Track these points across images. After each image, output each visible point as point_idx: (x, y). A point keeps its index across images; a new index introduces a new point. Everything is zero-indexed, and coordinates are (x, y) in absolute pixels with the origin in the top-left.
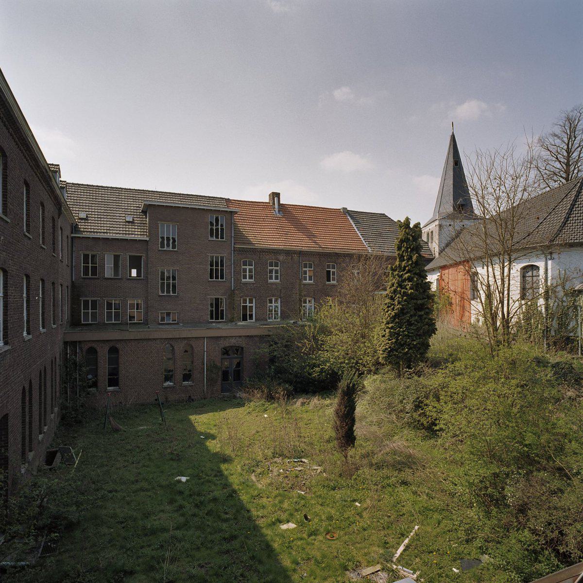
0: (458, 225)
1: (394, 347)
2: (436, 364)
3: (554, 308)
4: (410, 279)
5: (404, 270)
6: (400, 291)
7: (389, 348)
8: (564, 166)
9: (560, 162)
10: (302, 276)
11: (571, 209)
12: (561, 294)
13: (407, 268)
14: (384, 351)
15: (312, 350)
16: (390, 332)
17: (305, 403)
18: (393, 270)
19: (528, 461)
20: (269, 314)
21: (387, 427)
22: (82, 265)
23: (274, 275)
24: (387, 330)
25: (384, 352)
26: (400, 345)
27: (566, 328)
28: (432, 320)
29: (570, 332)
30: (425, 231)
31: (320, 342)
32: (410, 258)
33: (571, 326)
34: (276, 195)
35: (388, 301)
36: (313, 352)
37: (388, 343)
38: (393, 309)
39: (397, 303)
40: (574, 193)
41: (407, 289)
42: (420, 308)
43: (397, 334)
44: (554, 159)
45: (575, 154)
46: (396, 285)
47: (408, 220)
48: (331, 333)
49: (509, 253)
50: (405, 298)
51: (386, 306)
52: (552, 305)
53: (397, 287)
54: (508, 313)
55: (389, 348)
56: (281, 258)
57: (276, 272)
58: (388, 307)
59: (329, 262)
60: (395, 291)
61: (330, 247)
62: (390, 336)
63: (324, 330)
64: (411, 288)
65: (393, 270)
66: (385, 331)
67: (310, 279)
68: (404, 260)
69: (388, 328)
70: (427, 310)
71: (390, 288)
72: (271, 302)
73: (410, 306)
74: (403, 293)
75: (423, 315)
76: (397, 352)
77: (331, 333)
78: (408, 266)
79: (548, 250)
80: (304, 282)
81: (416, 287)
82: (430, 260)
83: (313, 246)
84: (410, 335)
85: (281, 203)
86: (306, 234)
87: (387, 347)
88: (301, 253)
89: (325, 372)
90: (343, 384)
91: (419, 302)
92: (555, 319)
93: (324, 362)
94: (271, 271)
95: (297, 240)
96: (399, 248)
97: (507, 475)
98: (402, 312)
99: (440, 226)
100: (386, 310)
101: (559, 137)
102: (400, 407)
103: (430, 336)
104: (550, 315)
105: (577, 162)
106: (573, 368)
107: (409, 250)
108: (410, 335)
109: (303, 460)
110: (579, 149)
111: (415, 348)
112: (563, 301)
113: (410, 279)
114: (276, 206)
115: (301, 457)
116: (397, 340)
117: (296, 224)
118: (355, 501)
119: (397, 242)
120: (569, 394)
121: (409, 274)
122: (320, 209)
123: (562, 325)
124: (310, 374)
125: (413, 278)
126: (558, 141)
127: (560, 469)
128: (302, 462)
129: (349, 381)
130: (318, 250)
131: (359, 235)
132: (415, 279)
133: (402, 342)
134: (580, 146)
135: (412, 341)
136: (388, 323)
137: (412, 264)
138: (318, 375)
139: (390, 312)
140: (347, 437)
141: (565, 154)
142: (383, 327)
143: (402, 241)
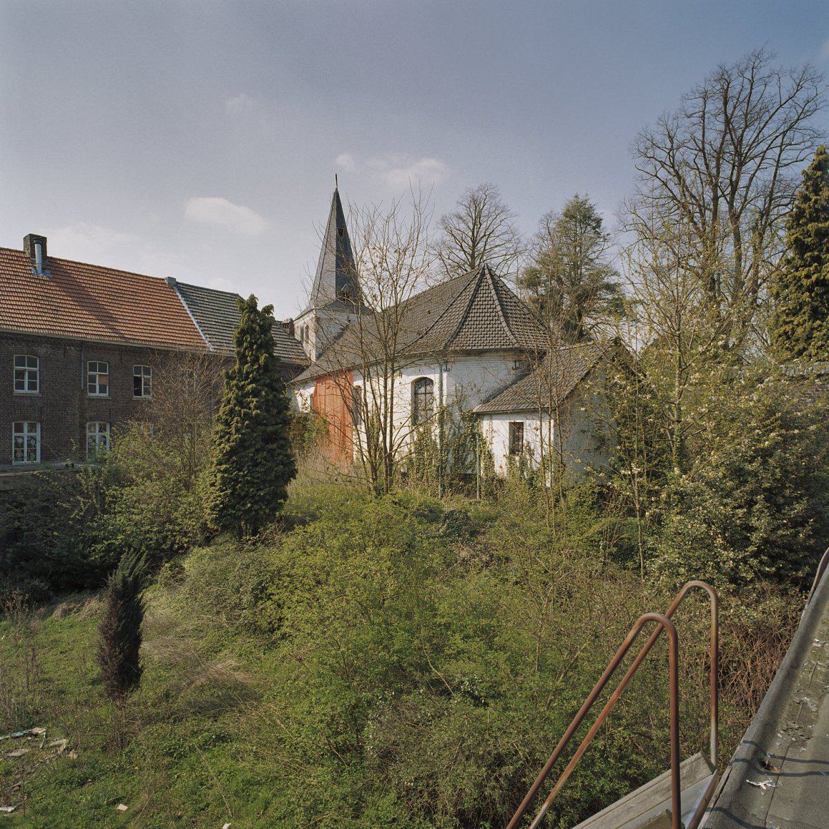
0: (342, 317)
1: (229, 501)
2: (289, 525)
3: (450, 436)
4: (255, 393)
5: (247, 378)
6: (240, 411)
7: (221, 504)
8: (469, 257)
9: (465, 252)
10: (85, 385)
11: (470, 306)
12: (457, 416)
13: (251, 375)
14: (212, 509)
15: (92, 512)
16: (222, 478)
17: (70, 610)
18: (230, 378)
19: (399, 676)
20: (16, 452)
21: (212, 636)
22: (38, 381)
23: (26, 381)
24: (219, 475)
25: (214, 510)
26: (238, 498)
27: (463, 464)
28: (289, 456)
29: (468, 469)
30: (299, 324)
31: (108, 499)
32: (256, 360)
33: (469, 460)
34: (37, 241)
35: (220, 427)
36: (93, 517)
37: (220, 496)
38: (228, 440)
39: (234, 431)
40: (474, 286)
41: (250, 409)
42: (269, 438)
43: (234, 480)
44: (458, 247)
45: (481, 245)
46: (233, 402)
47: (253, 299)
48: (132, 483)
49: (392, 363)
50: (247, 422)
51: (218, 436)
52: (447, 433)
53: (235, 405)
54: (391, 446)
55: (221, 504)
56: (42, 351)
57: (32, 375)
58: (221, 437)
59: (133, 363)
60: (231, 412)
61: (141, 338)
62: (223, 484)
63: (119, 478)
64: (256, 408)
65: (230, 378)
66: (216, 477)
67: (102, 390)
68: (247, 363)
69: (219, 471)
70: (282, 442)
71: (225, 406)
72: (19, 429)
73: (255, 435)
74: (244, 414)
75: (274, 450)
76: (234, 509)
77: (132, 483)
78: (252, 372)
79: (443, 357)
80: (91, 395)
81: (266, 405)
82: (300, 369)
83: (108, 334)
84: (256, 481)
85: (49, 255)
86: (96, 314)
87: (218, 502)
88: (83, 345)
89: (115, 550)
90: (116, 579)
91: (270, 429)
92: (451, 452)
93: (114, 534)
94: (20, 374)
95: (78, 323)
96: (240, 344)
97: (369, 703)
98: (242, 445)
99: (318, 320)
100: (217, 443)
101: (464, 221)
102: (234, 599)
103: (287, 481)
104: (445, 447)
105: (483, 254)
106: (468, 518)
107: (255, 346)
108: (256, 481)
109: (37, 730)
110: (484, 239)
111: (263, 502)
112: (459, 428)
113: (255, 393)
114: (38, 259)
115: (31, 727)
116: (234, 490)
117: (76, 295)
118: (118, 801)
119: (236, 333)
120: (463, 554)
121: (254, 385)
122: (128, 275)
123: (459, 460)
124: (85, 557)
125: (260, 391)
126: (462, 226)
127: (438, 682)
128: (31, 735)
129: (128, 571)
130: (116, 341)
131: (195, 323)
132: (263, 393)
133: (242, 494)
134: (485, 235)
135: (258, 490)
136: (220, 464)
137: (258, 369)
138: (101, 557)
139: (223, 445)
140: (124, 669)
141: (471, 243)
142: (213, 470)
143: (243, 332)
